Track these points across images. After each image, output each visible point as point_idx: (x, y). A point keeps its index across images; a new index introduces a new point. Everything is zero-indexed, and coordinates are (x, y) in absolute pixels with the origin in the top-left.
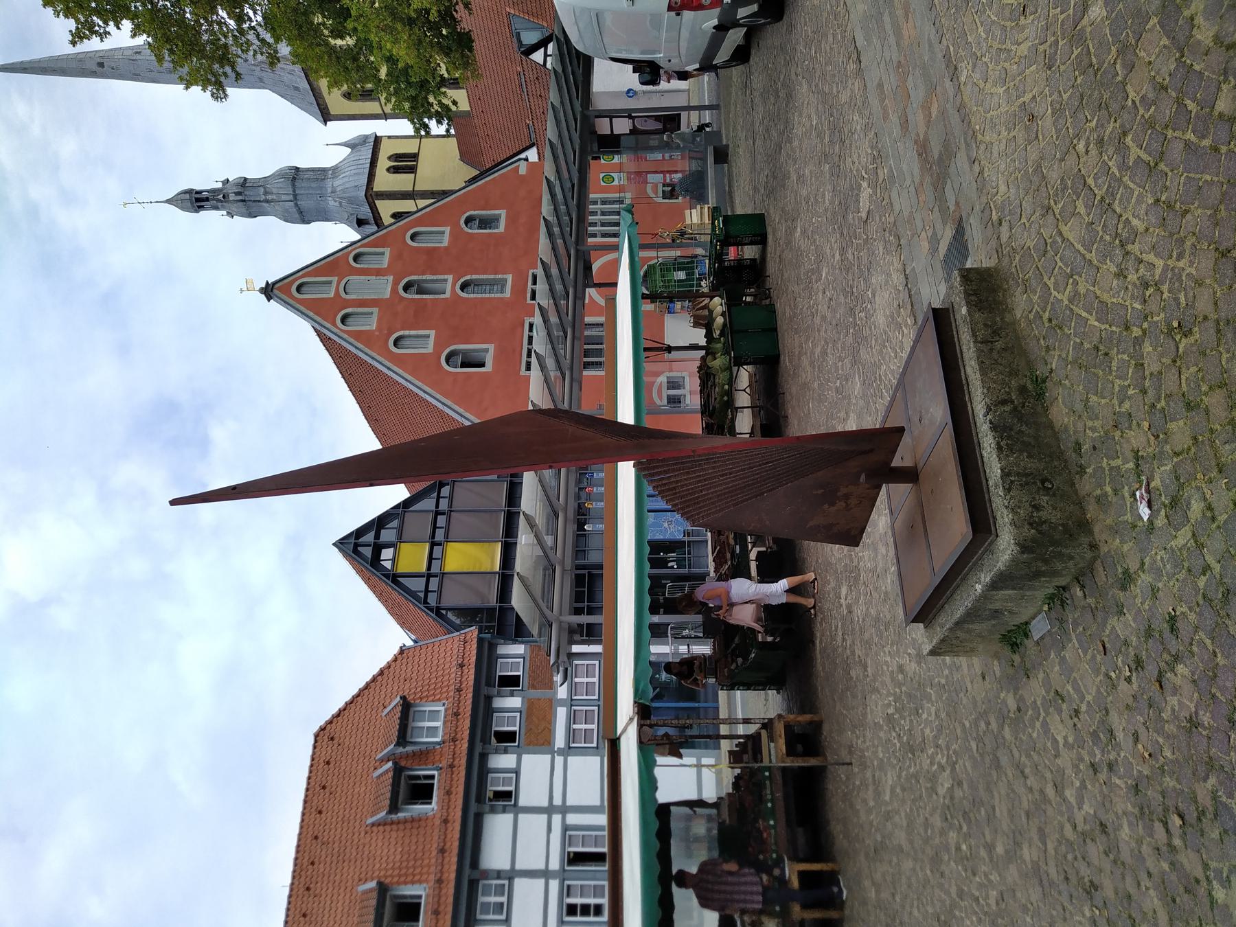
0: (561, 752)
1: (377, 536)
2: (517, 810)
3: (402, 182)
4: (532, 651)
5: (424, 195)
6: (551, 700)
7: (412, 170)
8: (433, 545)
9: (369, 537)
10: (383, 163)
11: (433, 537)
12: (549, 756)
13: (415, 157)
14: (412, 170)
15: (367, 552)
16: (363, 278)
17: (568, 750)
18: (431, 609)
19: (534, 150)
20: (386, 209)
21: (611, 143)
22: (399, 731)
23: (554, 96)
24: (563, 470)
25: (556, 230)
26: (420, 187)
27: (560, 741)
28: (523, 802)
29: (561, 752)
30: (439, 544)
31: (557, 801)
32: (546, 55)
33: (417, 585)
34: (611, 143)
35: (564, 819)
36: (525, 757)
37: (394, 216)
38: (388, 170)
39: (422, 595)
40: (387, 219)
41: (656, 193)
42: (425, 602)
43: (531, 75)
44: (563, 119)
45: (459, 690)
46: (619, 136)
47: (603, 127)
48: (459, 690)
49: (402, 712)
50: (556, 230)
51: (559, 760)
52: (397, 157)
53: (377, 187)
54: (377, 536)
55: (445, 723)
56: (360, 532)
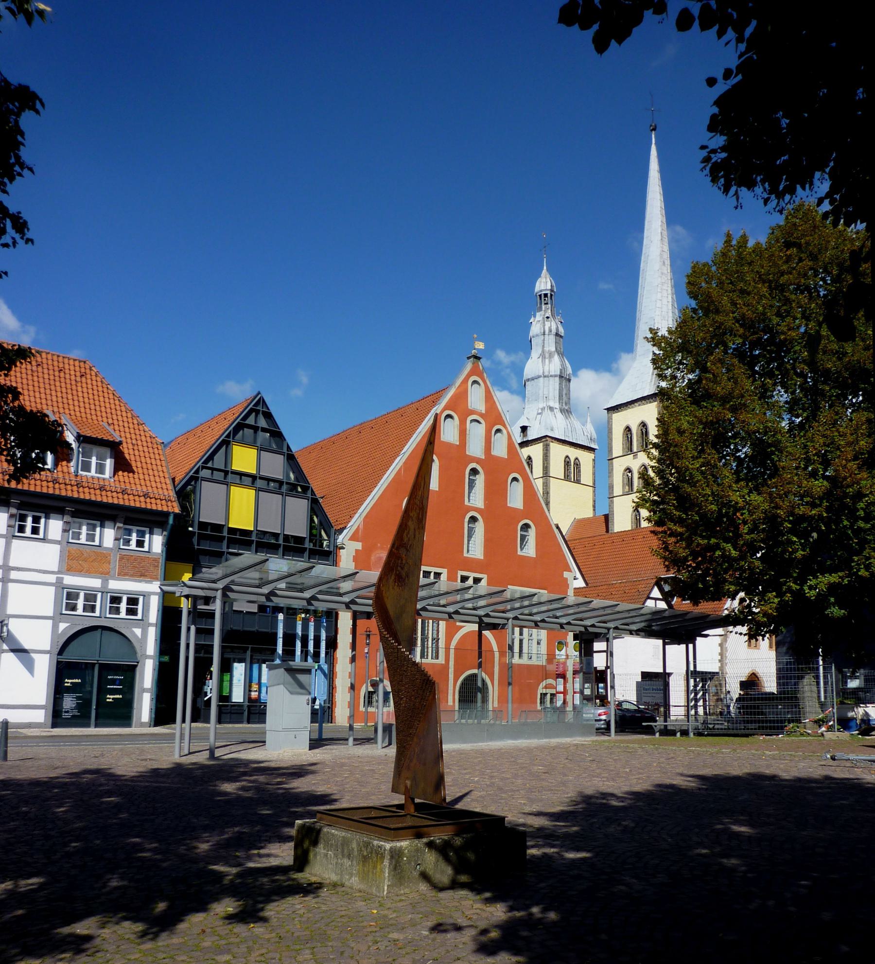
0: (59, 581)
1: (264, 430)
2: (10, 537)
3: (557, 468)
4: (155, 560)
5: (546, 485)
6: (108, 573)
7: (567, 478)
8: (254, 478)
9: (262, 423)
10: (573, 453)
11: (261, 478)
12: (56, 570)
13: (578, 481)
14: (567, 478)
15: (251, 421)
16: (645, 737)
17: (59, 585)
18: (197, 472)
19: (583, 585)
20: (535, 452)
21: (586, 651)
22: (90, 437)
23: (624, 606)
24: (370, 602)
25: (526, 603)
26: (553, 484)
27: (70, 580)
28: (15, 542)
29: (59, 581)
30: (253, 483)
31: (14, 575)
32: (656, 599)
33: (218, 461)
34: (586, 651)
35: (154, 593)
36: (57, 548)
37: (529, 458)
38: (567, 457)
39: (210, 465)
40: (525, 452)
41: (546, 687)
42: (203, 468)
43: (641, 587)
44: (606, 612)
45: (124, 492)
46: (592, 656)
47: (599, 646)
48: (124, 492)
49: (108, 441)
50: (526, 603)
51: (52, 578)
52: (577, 464)
53: (554, 447)
54: (264, 430)
55: (93, 478)
56: (268, 416)
